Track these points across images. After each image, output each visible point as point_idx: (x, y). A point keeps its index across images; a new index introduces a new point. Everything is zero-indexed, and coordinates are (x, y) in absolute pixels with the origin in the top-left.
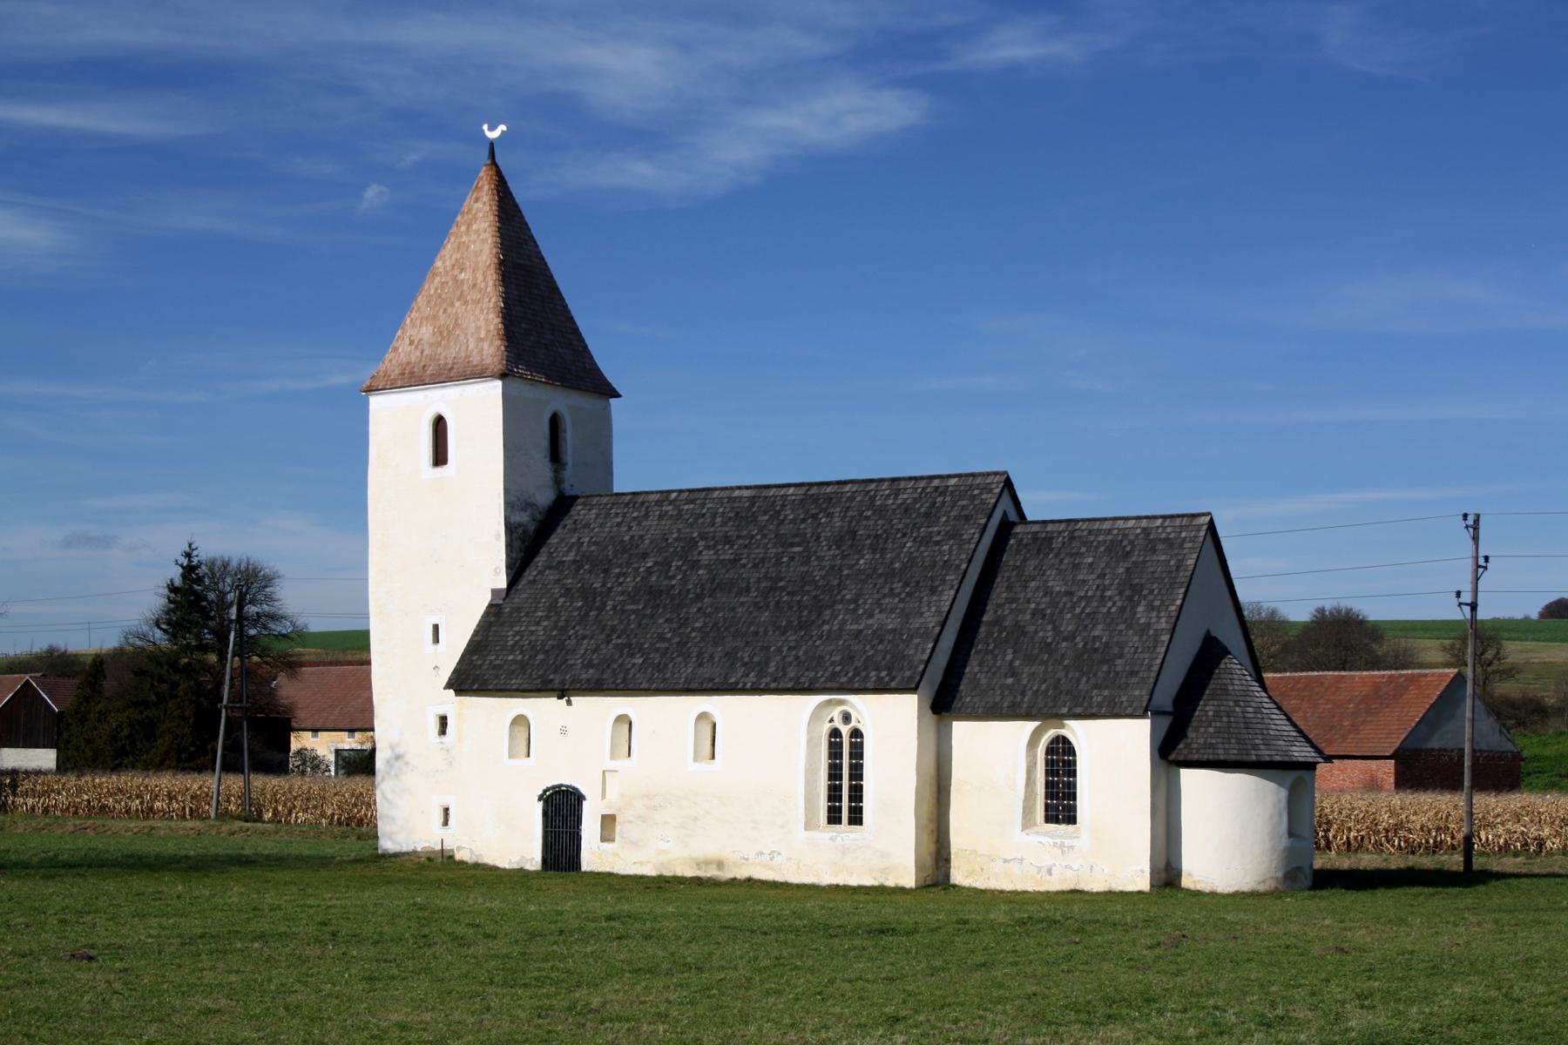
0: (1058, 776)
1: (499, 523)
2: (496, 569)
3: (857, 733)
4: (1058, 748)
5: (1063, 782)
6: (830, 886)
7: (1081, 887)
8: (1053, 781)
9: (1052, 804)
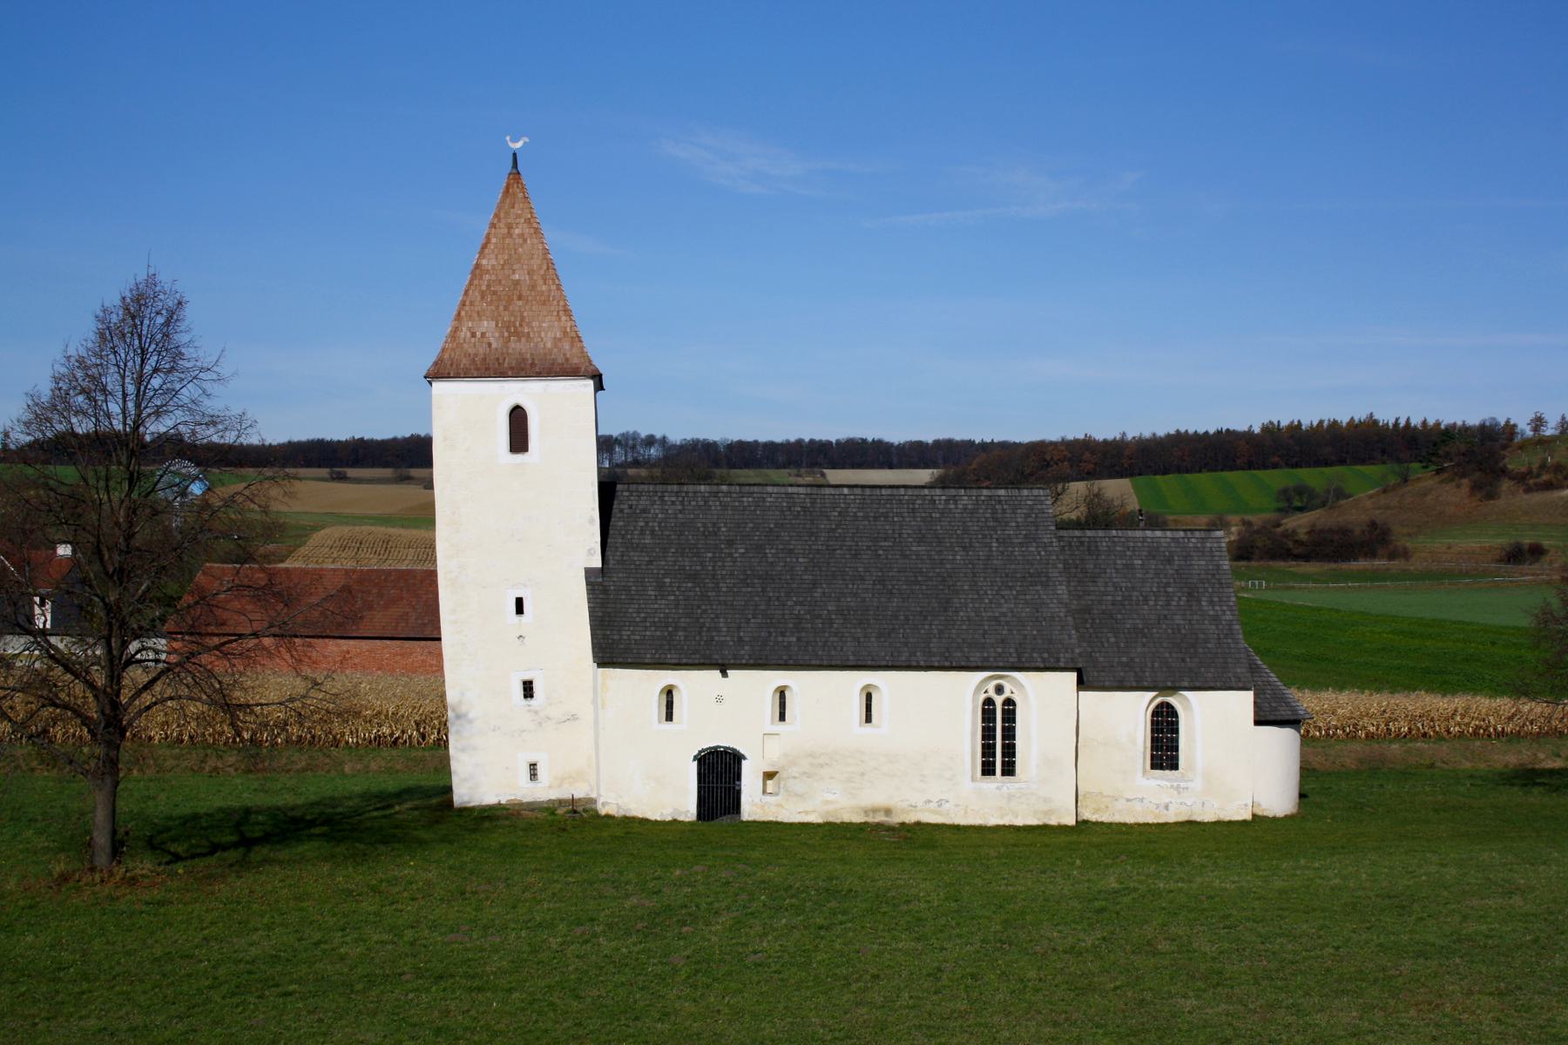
0: (1162, 733)
1: (593, 509)
2: (589, 550)
3: (1009, 702)
4: (1162, 712)
5: (1167, 738)
7: (1193, 818)
9: (1157, 755)
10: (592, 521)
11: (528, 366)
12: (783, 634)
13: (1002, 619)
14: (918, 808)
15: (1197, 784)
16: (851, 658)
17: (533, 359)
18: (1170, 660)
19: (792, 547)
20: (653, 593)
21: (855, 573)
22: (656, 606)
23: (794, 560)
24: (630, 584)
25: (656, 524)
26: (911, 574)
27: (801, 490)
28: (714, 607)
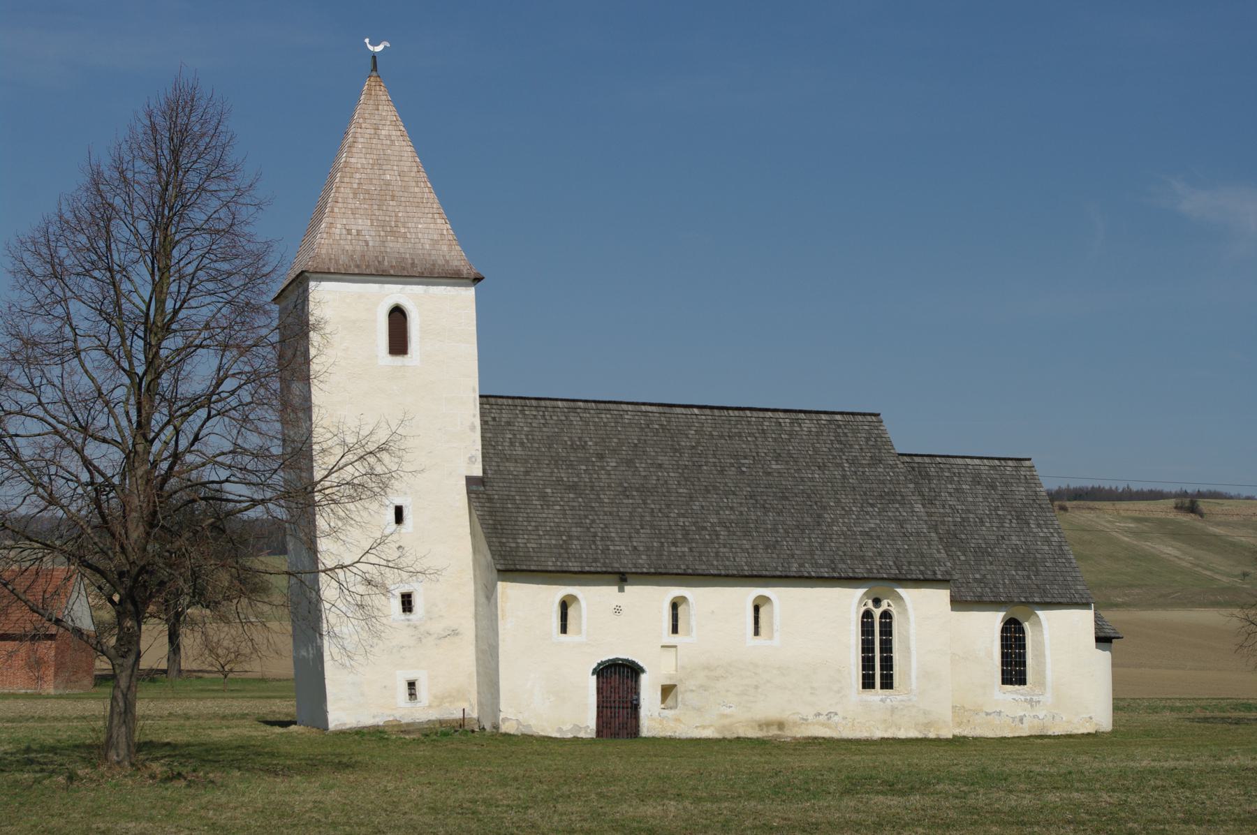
0: (1011, 648)
1: (474, 416)
3: (886, 615)
5: (1015, 653)
6: (884, 740)
8: (1007, 653)
10: (473, 428)
11: (409, 266)
12: (674, 544)
13: (873, 533)
14: (810, 721)
15: (1048, 698)
16: (746, 568)
17: (413, 259)
18: (1017, 577)
19: (659, 462)
20: (537, 503)
21: (727, 489)
22: (544, 515)
23: (666, 474)
24: (513, 493)
25: (523, 437)
26: (778, 490)
27: (654, 409)
28: (601, 517)
